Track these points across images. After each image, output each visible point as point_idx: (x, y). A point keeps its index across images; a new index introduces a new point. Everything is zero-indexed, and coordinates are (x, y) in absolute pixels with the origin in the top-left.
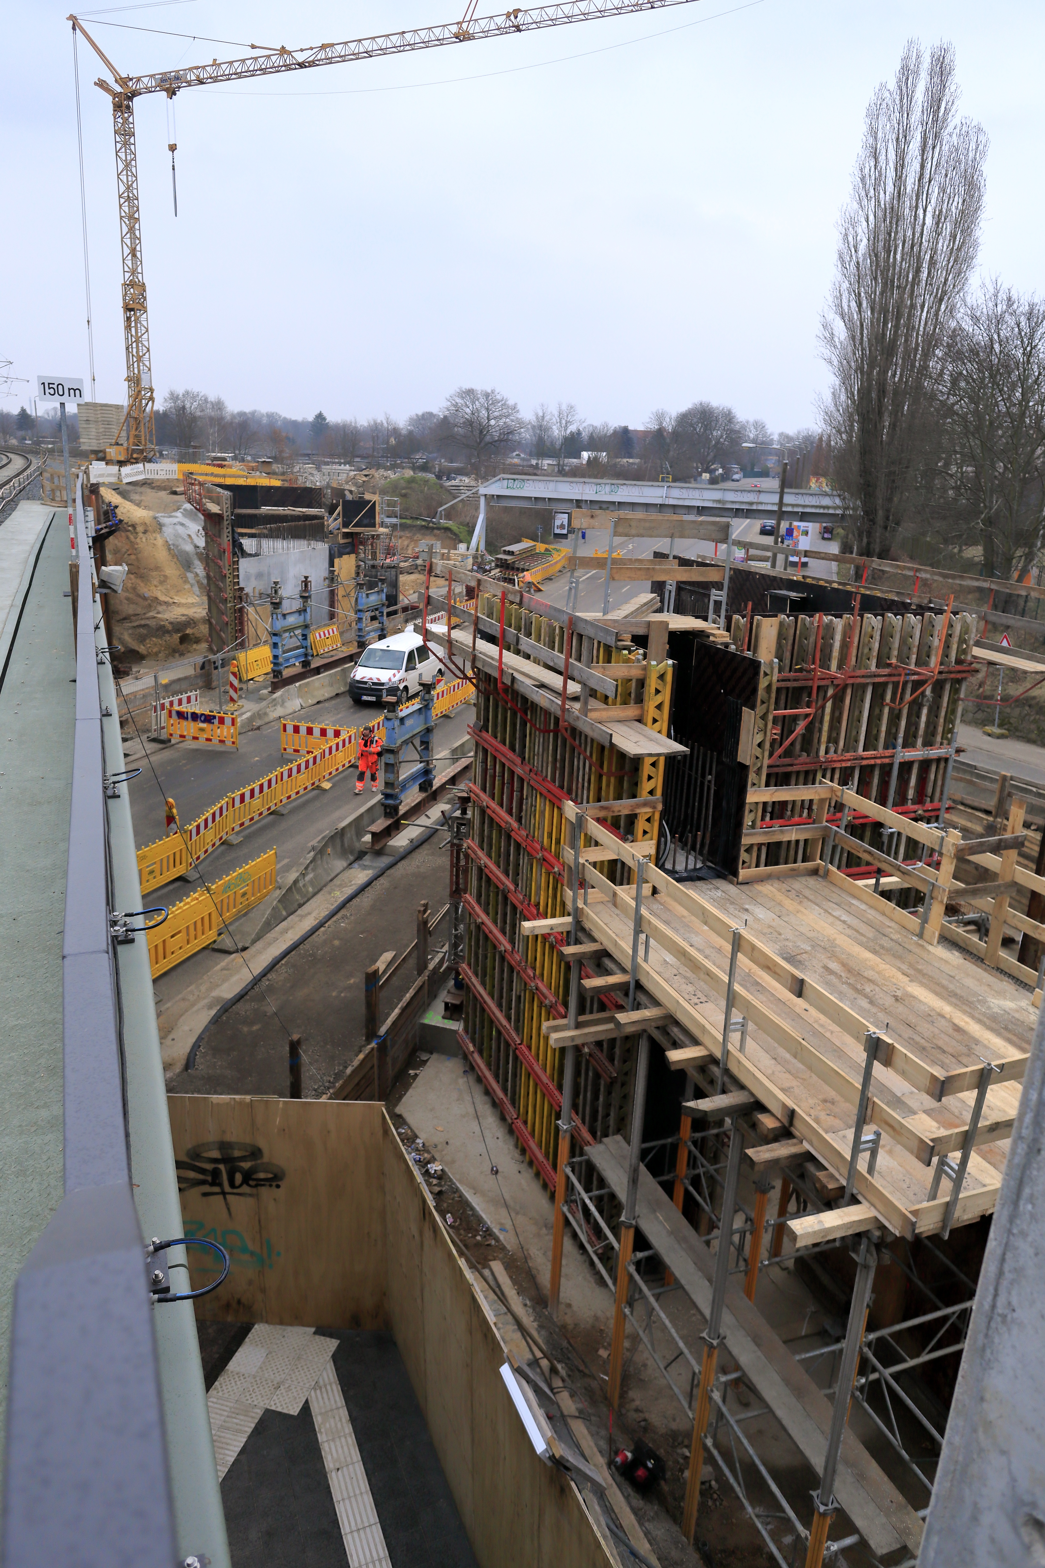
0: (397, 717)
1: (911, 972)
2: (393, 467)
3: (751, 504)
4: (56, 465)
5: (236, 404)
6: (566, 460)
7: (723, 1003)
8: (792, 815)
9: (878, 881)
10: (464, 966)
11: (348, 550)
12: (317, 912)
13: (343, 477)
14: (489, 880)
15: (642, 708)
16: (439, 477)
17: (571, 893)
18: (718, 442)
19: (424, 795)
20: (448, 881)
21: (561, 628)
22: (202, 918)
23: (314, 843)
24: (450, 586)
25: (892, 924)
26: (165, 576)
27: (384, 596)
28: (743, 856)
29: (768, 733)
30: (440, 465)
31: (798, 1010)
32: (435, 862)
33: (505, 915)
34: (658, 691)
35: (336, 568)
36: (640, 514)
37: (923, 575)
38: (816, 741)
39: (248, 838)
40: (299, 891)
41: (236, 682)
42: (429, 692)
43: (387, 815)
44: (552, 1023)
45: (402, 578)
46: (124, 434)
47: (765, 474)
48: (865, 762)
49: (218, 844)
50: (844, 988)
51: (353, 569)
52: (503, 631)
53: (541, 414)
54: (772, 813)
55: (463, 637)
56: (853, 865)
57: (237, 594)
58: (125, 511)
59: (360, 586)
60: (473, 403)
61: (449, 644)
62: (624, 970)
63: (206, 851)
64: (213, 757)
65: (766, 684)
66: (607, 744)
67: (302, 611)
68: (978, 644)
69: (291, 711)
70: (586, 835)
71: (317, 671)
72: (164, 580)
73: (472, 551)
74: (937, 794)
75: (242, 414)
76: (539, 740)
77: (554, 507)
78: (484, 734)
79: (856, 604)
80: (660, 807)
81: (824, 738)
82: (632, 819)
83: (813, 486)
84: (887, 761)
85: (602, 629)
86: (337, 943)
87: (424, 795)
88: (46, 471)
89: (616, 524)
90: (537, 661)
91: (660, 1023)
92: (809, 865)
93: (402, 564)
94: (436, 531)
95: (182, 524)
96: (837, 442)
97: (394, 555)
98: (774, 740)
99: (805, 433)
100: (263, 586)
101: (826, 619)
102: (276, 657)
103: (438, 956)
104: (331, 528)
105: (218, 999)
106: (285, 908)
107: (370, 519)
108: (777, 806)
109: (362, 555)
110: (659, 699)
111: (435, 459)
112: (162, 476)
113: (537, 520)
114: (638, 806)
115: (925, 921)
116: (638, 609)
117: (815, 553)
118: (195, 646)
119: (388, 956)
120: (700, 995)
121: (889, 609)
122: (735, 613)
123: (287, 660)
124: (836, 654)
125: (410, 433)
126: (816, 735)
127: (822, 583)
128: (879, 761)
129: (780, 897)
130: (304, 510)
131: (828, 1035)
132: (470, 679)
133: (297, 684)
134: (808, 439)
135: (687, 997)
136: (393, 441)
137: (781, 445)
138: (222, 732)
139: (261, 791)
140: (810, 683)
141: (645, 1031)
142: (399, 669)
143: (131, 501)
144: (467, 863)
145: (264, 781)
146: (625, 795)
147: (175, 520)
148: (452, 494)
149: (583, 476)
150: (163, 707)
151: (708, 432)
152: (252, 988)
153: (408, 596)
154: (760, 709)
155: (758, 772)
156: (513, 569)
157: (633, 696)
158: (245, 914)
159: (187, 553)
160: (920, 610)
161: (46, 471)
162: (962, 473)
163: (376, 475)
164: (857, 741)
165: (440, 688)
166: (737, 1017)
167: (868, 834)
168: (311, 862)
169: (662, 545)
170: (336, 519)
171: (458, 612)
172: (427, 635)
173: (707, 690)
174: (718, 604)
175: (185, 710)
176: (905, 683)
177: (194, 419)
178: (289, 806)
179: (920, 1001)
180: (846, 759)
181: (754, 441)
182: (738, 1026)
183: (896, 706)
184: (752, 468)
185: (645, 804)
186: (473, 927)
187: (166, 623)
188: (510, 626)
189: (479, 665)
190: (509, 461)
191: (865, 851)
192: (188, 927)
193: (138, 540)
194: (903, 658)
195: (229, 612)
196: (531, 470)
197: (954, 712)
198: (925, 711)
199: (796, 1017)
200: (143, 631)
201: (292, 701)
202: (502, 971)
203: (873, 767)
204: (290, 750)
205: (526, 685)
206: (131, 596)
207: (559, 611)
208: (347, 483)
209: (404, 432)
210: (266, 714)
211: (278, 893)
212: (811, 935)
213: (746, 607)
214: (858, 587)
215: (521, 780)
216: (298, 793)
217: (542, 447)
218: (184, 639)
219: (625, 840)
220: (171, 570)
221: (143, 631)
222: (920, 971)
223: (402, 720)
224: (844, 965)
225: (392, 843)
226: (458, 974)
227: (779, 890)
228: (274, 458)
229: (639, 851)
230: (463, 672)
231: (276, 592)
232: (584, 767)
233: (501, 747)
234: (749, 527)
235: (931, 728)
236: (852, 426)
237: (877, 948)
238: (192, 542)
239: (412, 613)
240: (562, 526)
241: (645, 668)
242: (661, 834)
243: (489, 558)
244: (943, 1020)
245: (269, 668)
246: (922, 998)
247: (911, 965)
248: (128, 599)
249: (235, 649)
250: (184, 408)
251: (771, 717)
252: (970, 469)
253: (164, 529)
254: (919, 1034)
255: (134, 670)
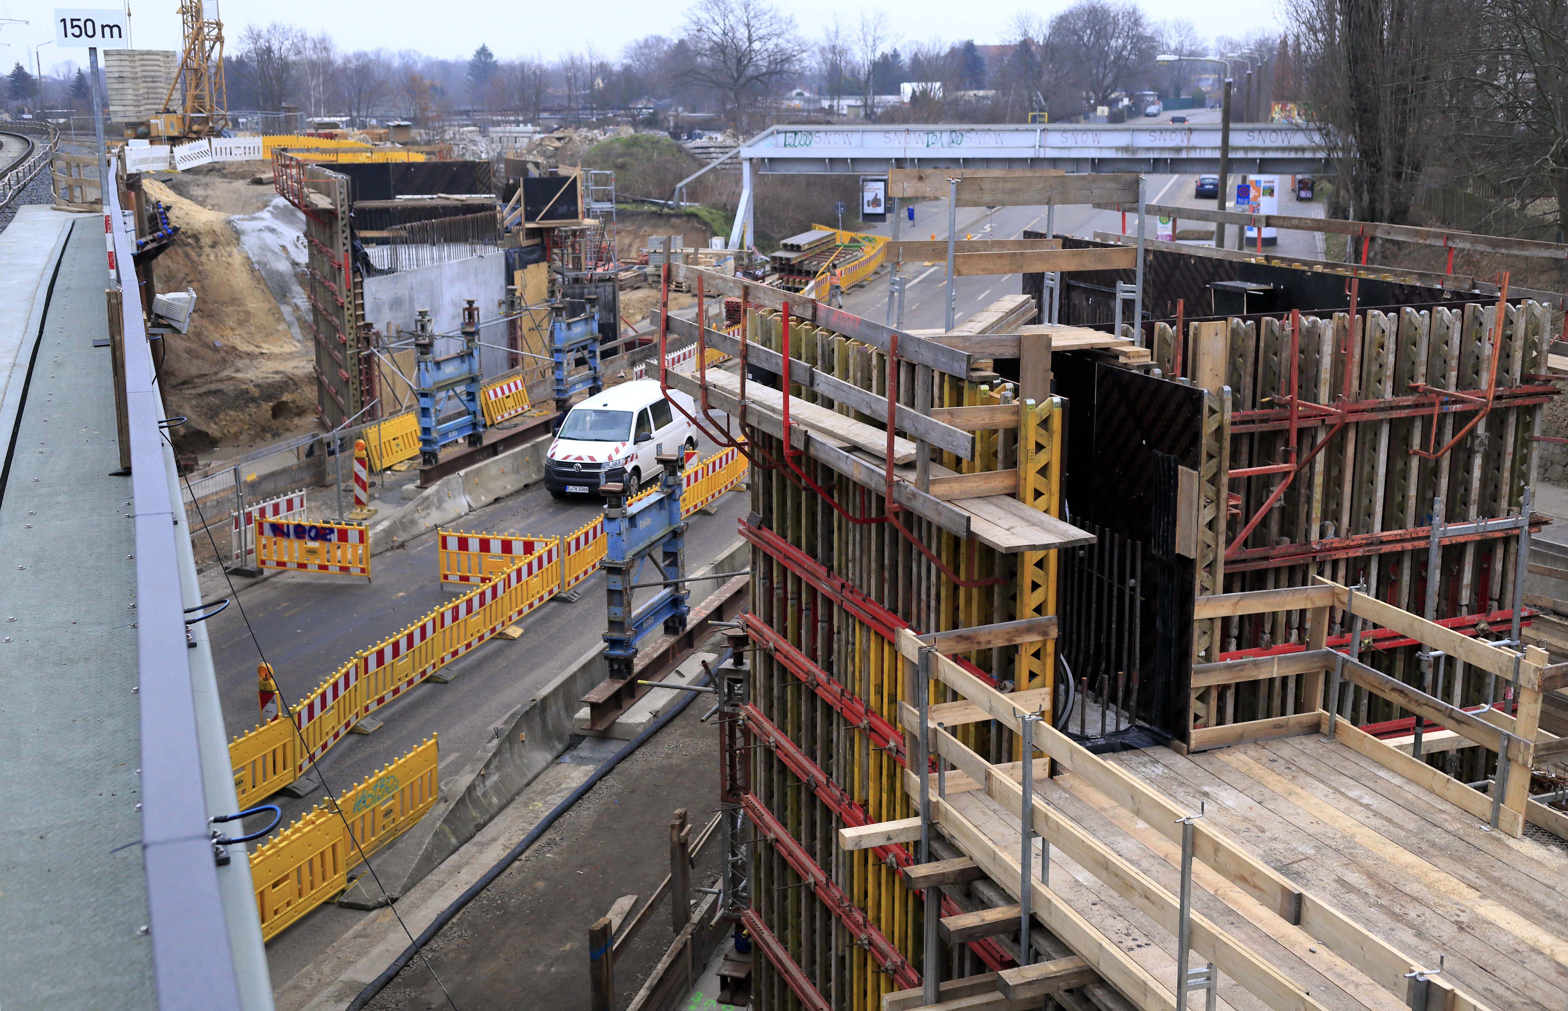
0: (624, 516)
1: (1482, 882)
2: (602, 124)
3: (1179, 149)
4: (73, 149)
5: (349, 42)
6: (877, 99)
7: (1174, 946)
8: (1273, 641)
9: (1418, 739)
10: (750, 913)
11: (535, 256)
12: (507, 836)
13: (523, 143)
14: (783, 768)
15: (1017, 474)
16: (675, 135)
17: (917, 779)
18: (1119, 56)
19: (672, 639)
20: (717, 777)
21: (881, 356)
22: (322, 854)
23: (499, 724)
24: (700, 305)
25: (1447, 807)
26: (247, 313)
27: (595, 326)
28: (1195, 706)
29: (1223, 506)
30: (676, 117)
31: (1298, 952)
32: (696, 746)
33: (813, 824)
34: (1039, 447)
35: (518, 285)
36: (997, 172)
37: (1459, 244)
38: (1303, 517)
39: (391, 722)
40: (476, 803)
41: (363, 474)
42: (673, 473)
43: (614, 674)
44: (897, 995)
45: (624, 297)
46: (177, 95)
47: (1198, 102)
48: (1386, 549)
49: (343, 733)
50: (1374, 913)
51: (545, 286)
52: (788, 365)
53: (833, 29)
54: (1239, 638)
55: (724, 379)
56: (1378, 715)
57: (362, 334)
58: (181, 214)
59: (557, 311)
60: (725, 17)
61: (705, 393)
62: (1010, 900)
63: (324, 746)
64: (330, 594)
65: (1214, 426)
66: (963, 534)
67: (466, 356)
68: (1556, 349)
69: (453, 515)
70: (937, 681)
71: (493, 450)
72: (245, 319)
73: (733, 248)
74: (1509, 596)
75: (359, 56)
76: (854, 535)
77: (862, 171)
78: (766, 533)
79: (1353, 295)
80: (1054, 633)
81: (1317, 512)
82: (1010, 654)
83: (1276, 116)
84: (1421, 544)
85: (944, 351)
86: (540, 885)
87: (672, 639)
88: (59, 158)
89: (959, 188)
90: (844, 411)
91: (1074, 983)
92: (1305, 717)
93: (623, 275)
94: (673, 220)
95: (272, 230)
96: (1312, 45)
97: (609, 260)
98: (1233, 516)
99: (1258, 36)
100: (401, 319)
101: (1306, 321)
102: (426, 431)
103: (707, 901)
104: (507, 223)
105: (351, 985)
106: (454, 833)
107: (568, 206)
108: (1247, 628)
109: (559, 263)
110: (1042, 459)
111: (669, 107)
112: (239, 156)
113: (836, 194)
114: (1019, 632)
115: (1501, 798)
116: (1001, 319)
117: (1285, 221)
118: (296, 421)
119: (625, 903)
120: (1136, 934)
121: (1408, 301)
122: (1159, 319)
123: (445, 434)
124: (1325, 374)
125: (627, 69)
126: (1303, 509)
127: (1296, 266)
128: (1408, 546)
129: (1258, 770)
130: (464, 197)
131: (1350, 989)
132: (740, 446)
133: (462, 472)
134: (1263, 45)
135: (1115, 938)
136: (599, 83)
137: (1222, 55)
138: (344, 554)
139: (410, 644)
140: (1286, 425)
141: (1048, 997)
142: (624, 441)
143: (190, 198)
144: (747, 742)
145: (415, 628)
146: (996, 616)
147: (260, 224)
148: (697, 160)
149: (905, 121)
150: (249, 518)
151: (1102, 42)
152: (406, 965)
153: (635, 324)
154: (1207, 468)
155: (1211, 567)
156: (800, 272)
157: (1000, 456)
158: (388, 845)
159: (281, 274)
160: (1458, 300)
161: (59, 158)
162: (1516, 85)
163: (576, 137)
164: (1370, 514)
165: (691, 467)
166: (1197, 964)
167: (1400, 665)
168: (495, 755)
169: (1034, 217)
170: (514, 209)
171: (715, 339)
172: (667, 380)
173: (1119, 440)
174: (1128, 305)
175: (283, 521)
176: (1443, 417)
177: (285, 66)
178: (456, 668)
179: (1500, 929)
180: (1355, 545)
181: (1176, 52)
182: (1202, 980)
183: (1430, 455)
184: (1178, 95)
185: (1030, 629)
186: (761, 847)
187: (251, 387)
188: (800, 358)
189: (752, 421)
190: (786, 103)
191: (1394, 689)
192: (299, 870)
193: (204, 259)
194: (1436, 377)
195: (349, 363)
196: (821, 116)
197: (1525, 459)
198: (1478, 461)
199: (1296, 963)
200: (214, 400)
201: (455, 501)
202: (813, 918)
203: (1400, 554)
204: (454, 578)
205: (828, 449)
206: (194, 346)
207: (876, 327)
208: (529, 152)
209: (617, 68)
210: (413, 522)
211: (442, 809)
212: (1312, 829)
213: (1174, 305)
214: (1356, 270)
215: (829, 603)
216: (468, 646)
217: (838, 80)
218: (279, 410)
219: (1002, 689)
220: (256, 303)
221: (214, 400)
222: (1497, 881)
223: (633, 519)
224: (1370, 876)
225: (624, 719)
226: (740, 927)
227: (1258, 760)
228: (413, 119)
229: (1024, 704)
230: (727, 434)
231: (423, 327)
232: (929, 576)
233: (793, 551)
234: (1178, 186)
235: (1492, 488)
236: (1332, 20)
237: (1424, 846)
238: (288, 257)
239: (641, 350)
240: (876, 202)
241: (1017, 411)
242: (1059, 678)
243: (761, 257)
244: (1539, 959)
245: (416, 449)
246: (1502, 924)
247: (1481, 872)
248: (188, 351)
249: (361, 420)
250: (269, 50)
251: (1225, 480)
252: (1527, 76)
253: (243, 238)
254: (1501, 981)
255: (201, 462)
